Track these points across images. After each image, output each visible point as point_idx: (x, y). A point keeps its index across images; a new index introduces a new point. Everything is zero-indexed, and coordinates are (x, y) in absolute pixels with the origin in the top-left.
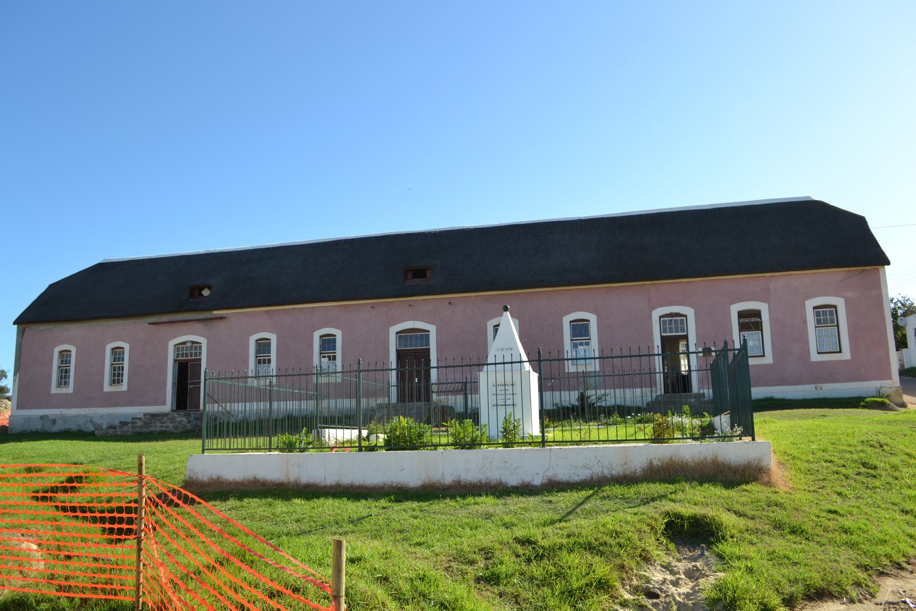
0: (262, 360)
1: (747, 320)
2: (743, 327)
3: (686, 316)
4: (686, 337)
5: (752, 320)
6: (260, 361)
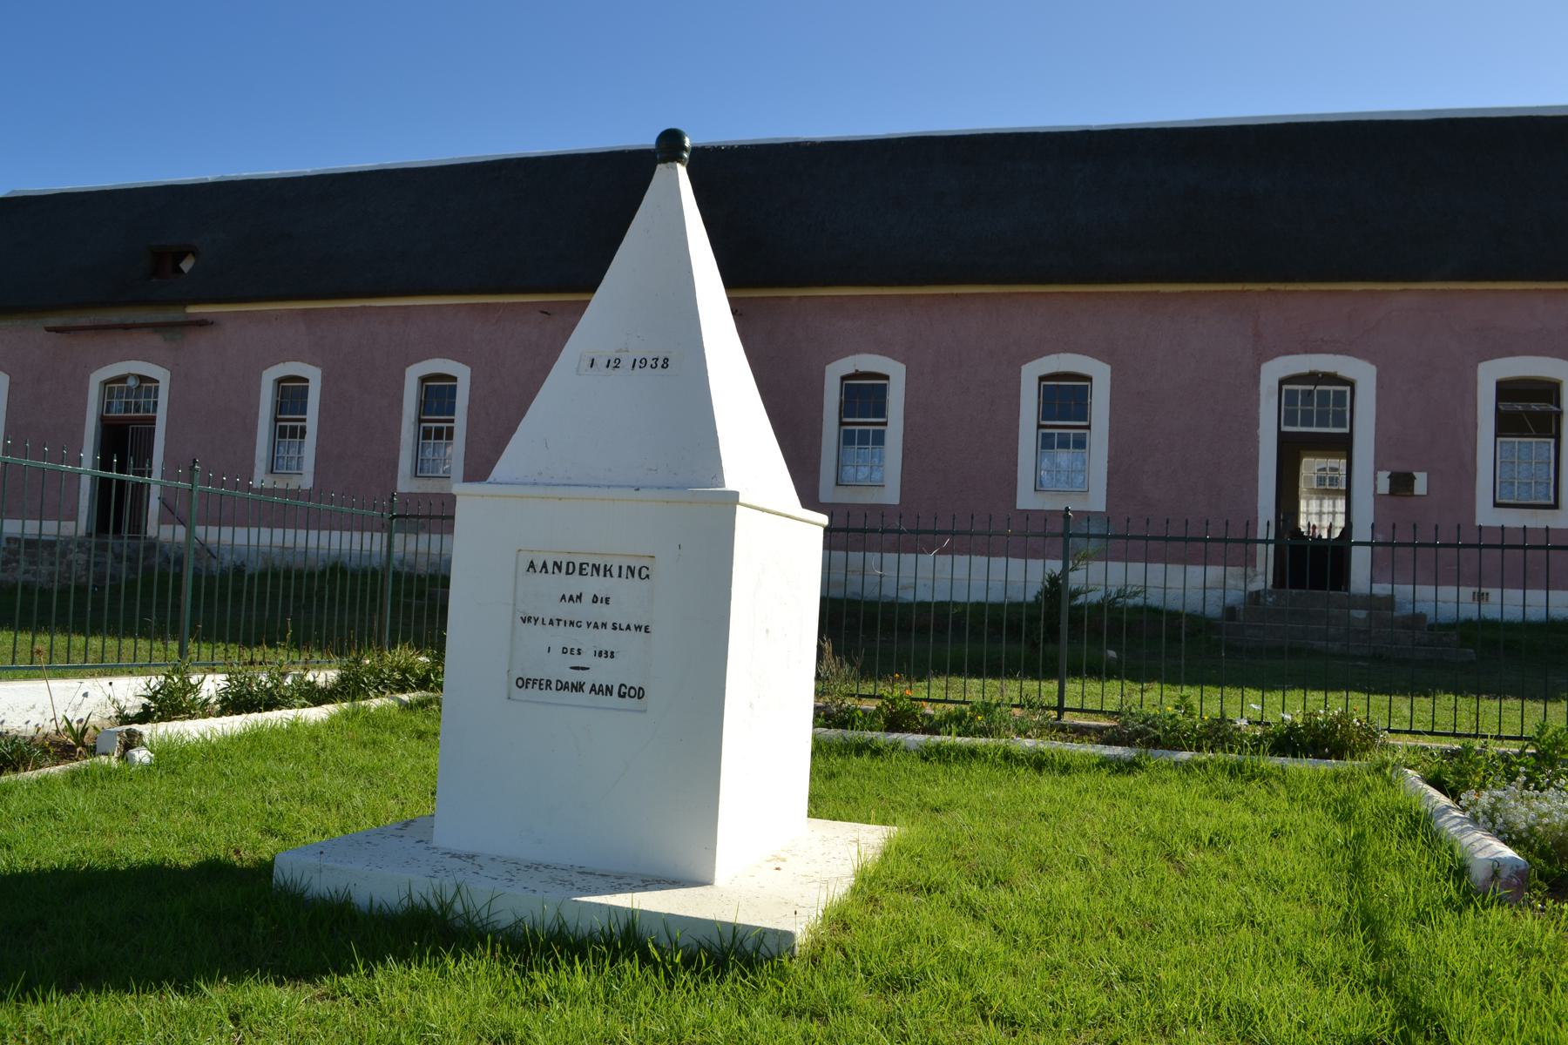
0: (288, 432)
1: (1519, 407)
2: (1506, 425)
3: (1351, 384)
4: (1342, 445)
5: (1535, 407)
6: (283, 429)
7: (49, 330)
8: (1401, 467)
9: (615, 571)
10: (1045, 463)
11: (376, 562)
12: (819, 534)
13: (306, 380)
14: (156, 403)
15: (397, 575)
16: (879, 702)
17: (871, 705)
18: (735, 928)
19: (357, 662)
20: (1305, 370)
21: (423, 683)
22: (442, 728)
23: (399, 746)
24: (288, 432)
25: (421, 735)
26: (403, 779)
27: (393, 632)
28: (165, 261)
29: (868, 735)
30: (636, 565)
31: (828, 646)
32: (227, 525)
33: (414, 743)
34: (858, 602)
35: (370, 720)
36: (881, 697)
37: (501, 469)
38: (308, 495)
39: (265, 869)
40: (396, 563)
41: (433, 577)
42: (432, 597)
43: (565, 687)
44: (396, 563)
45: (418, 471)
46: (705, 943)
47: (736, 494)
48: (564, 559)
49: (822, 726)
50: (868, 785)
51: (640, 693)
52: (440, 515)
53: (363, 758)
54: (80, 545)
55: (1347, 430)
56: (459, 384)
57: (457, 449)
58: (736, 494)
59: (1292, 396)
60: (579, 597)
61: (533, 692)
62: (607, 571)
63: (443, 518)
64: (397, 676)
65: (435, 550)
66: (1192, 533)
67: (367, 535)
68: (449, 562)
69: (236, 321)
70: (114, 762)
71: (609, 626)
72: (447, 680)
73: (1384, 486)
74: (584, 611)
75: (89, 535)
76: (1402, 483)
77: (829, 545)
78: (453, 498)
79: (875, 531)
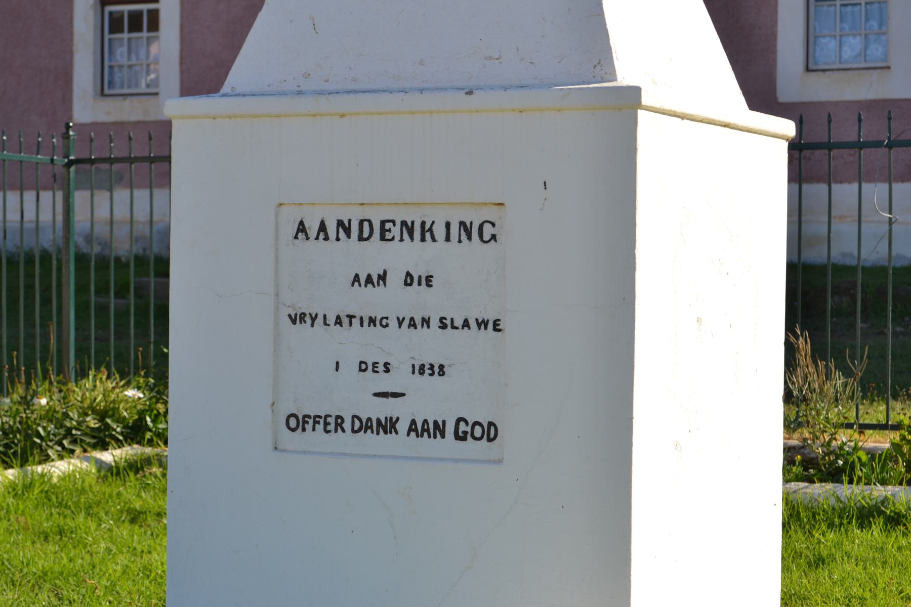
9: (440, 231)
11: (47, 240)
12: (781, 150)
15: (82, 260)
16: (895, 436)
17: (881, 442)
19: (26, 402)
21: (135, 432)
22: (169, 504)
23: (100, 536)
25: (135, 517)
26: (111, 589)
27: (82, 351)
29: (879, 491)
30: (474, 218)
31: (804, 345)
33: (125, 531)
34: (852, 270)
35: (53, 496)
36: (897, 427)
37: (240, 73)
40: (80, 240)
41: (141, 260)
42: (141, 292)
43: (365, 426)
44: (80, 240)
45: (105, 86)
47: (635, 92)
48: (354, 215)
49: (798, 479)
50: (883, 576)
51: (490, 432)
52: (147, 157)
53: (45, 557)
57: (167, 43)
58: (635, 92)
60: (383, 277)
61: (315, 437)
62: (427, 231)
63: (151, 160)
64: (92, 422)
65: (141, 214)
67: (30, 196)
68: (166, 234)
71: (435, 323)
72: (175, 426)
74: (392, 299)
77: (799, 173)
78: (166, 127)
79: (878, 144)
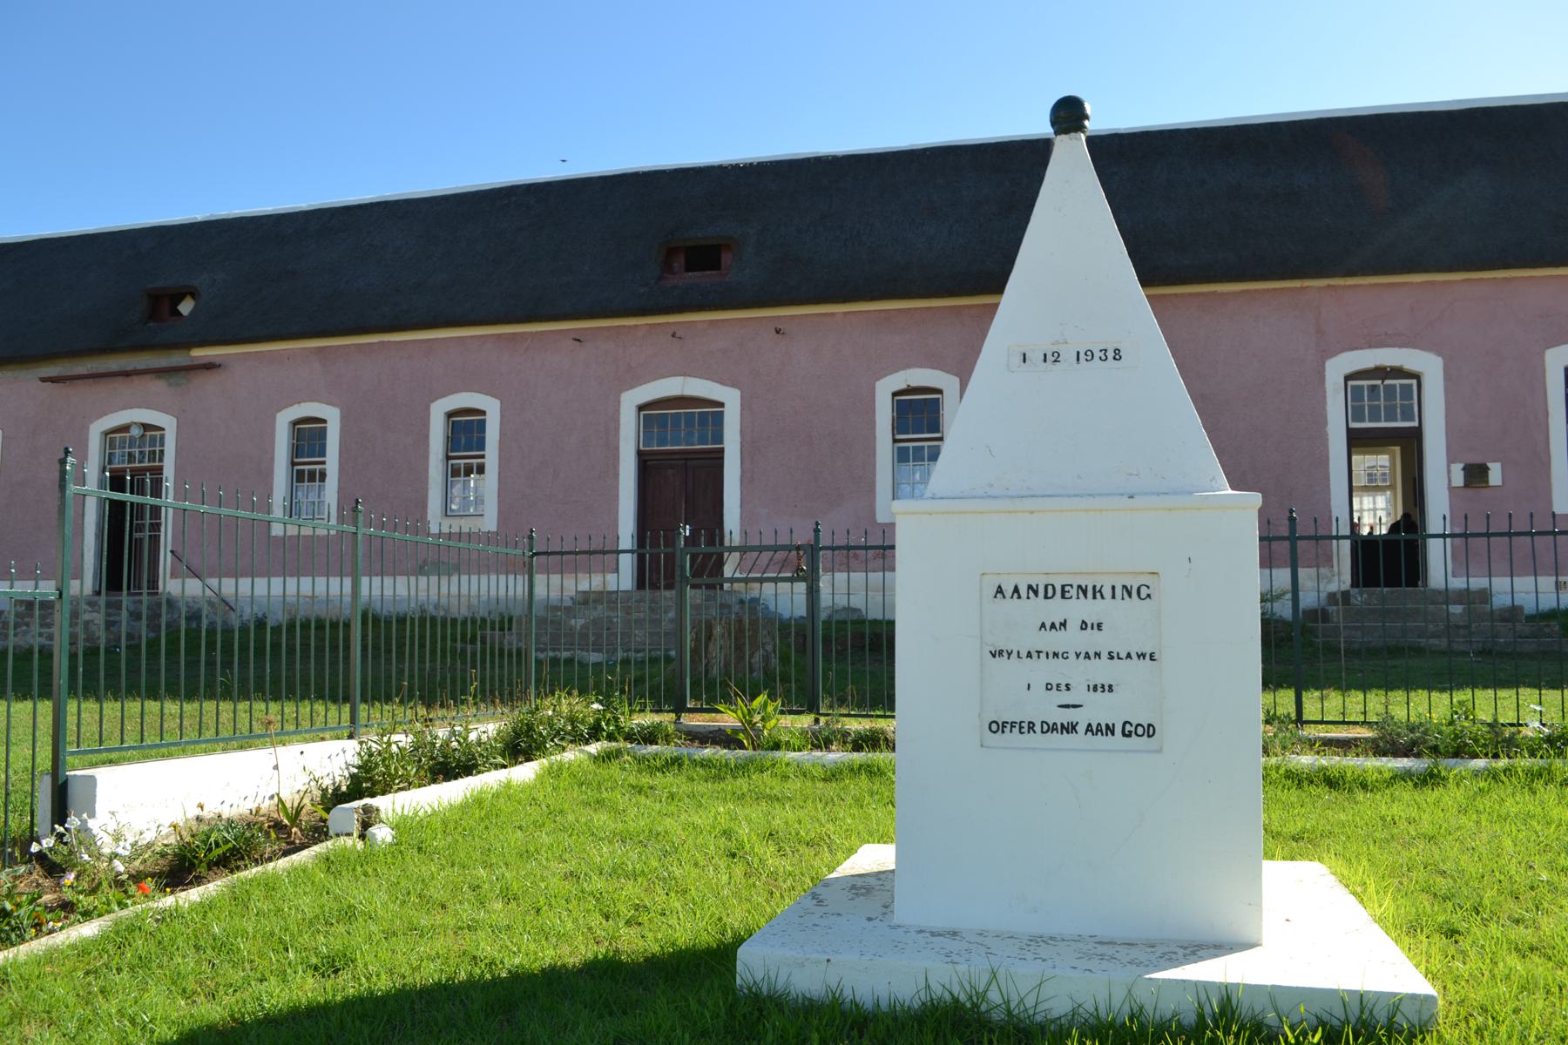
0: (306, 475)
3: (1417, 376)
6: (300, 474)
7: (43, 380)
8: (1476, 459)
9: (1107, 592)
10: (457, 490)
13: (324, 421)
14: (162, 452)
18: (1361, 996)
20: (1370, 365)
24: (306, 475)
28: (162, 303)
32: (261, 575)
38: (488, 538)
39: (711, 963)
43: (1053, 728)
46: (1326, 1017)
48: (1040, 582)
51: (1150, 731)
54: (91, 604)
55: (1416, 424)
56: (488, 418)
59: (1358, 391)
60: (1064, 624)
61: (1012, 737)
62: (1097, 592)
66: (838, 543)
69: (246, 363)
70: (353, 843)
71: (1105, 655)
73: (1458, 479)
74: (1072, 639)
75: (98, 593)
76: (1476, 474)
